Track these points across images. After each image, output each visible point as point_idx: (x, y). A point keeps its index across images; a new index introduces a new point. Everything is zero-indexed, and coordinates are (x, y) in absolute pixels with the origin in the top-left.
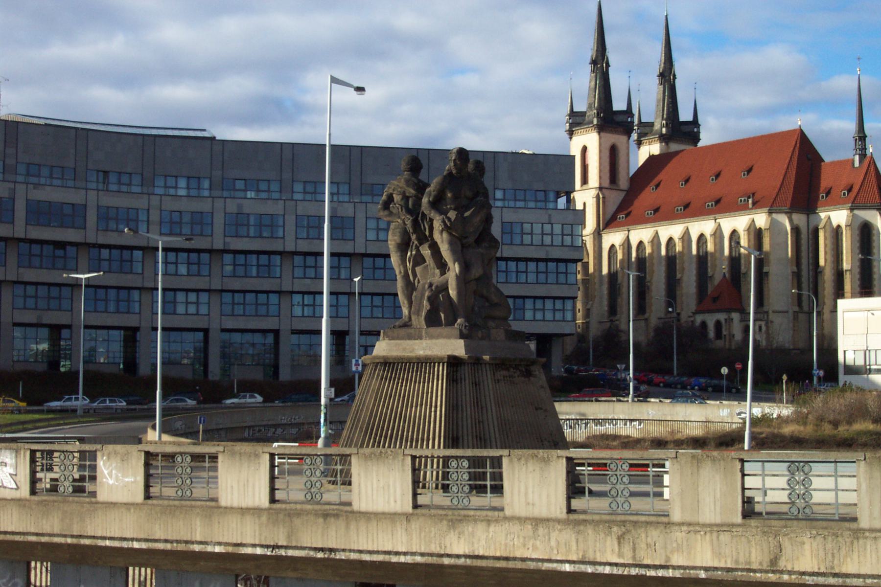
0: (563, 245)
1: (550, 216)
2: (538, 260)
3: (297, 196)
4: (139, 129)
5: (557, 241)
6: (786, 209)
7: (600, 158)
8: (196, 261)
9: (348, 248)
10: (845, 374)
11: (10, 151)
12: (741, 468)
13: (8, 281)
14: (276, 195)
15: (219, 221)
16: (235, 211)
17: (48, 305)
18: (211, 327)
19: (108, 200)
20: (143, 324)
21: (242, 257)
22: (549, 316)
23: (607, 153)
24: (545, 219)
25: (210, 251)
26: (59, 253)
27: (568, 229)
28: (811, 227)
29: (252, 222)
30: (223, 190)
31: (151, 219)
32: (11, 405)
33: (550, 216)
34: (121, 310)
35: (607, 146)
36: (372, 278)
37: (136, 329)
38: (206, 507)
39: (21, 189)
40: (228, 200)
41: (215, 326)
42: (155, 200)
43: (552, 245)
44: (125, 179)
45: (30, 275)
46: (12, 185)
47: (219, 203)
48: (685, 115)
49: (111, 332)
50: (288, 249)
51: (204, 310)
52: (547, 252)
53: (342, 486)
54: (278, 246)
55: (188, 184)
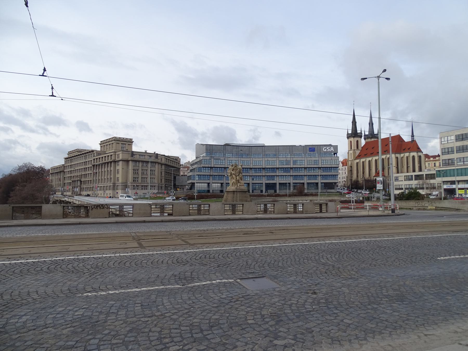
5: (333, 163)
6: (394, 153)
7: (291, 149)
10: (276, 183)
12: (312, 194)
20: (211, 182)
21: (296, 168)
23: (350, 143)
25: (263, 168)
28: (401, 157)
34: (408, 176)
37: (209, 183)
38: (46, 202)
45: (268, 174)
47: (264, 159)
48: (376, 132)
49: (218, 184)
50: (320, 167)
51: (248, 179)
53: (444, 201)
54: (289, 166)
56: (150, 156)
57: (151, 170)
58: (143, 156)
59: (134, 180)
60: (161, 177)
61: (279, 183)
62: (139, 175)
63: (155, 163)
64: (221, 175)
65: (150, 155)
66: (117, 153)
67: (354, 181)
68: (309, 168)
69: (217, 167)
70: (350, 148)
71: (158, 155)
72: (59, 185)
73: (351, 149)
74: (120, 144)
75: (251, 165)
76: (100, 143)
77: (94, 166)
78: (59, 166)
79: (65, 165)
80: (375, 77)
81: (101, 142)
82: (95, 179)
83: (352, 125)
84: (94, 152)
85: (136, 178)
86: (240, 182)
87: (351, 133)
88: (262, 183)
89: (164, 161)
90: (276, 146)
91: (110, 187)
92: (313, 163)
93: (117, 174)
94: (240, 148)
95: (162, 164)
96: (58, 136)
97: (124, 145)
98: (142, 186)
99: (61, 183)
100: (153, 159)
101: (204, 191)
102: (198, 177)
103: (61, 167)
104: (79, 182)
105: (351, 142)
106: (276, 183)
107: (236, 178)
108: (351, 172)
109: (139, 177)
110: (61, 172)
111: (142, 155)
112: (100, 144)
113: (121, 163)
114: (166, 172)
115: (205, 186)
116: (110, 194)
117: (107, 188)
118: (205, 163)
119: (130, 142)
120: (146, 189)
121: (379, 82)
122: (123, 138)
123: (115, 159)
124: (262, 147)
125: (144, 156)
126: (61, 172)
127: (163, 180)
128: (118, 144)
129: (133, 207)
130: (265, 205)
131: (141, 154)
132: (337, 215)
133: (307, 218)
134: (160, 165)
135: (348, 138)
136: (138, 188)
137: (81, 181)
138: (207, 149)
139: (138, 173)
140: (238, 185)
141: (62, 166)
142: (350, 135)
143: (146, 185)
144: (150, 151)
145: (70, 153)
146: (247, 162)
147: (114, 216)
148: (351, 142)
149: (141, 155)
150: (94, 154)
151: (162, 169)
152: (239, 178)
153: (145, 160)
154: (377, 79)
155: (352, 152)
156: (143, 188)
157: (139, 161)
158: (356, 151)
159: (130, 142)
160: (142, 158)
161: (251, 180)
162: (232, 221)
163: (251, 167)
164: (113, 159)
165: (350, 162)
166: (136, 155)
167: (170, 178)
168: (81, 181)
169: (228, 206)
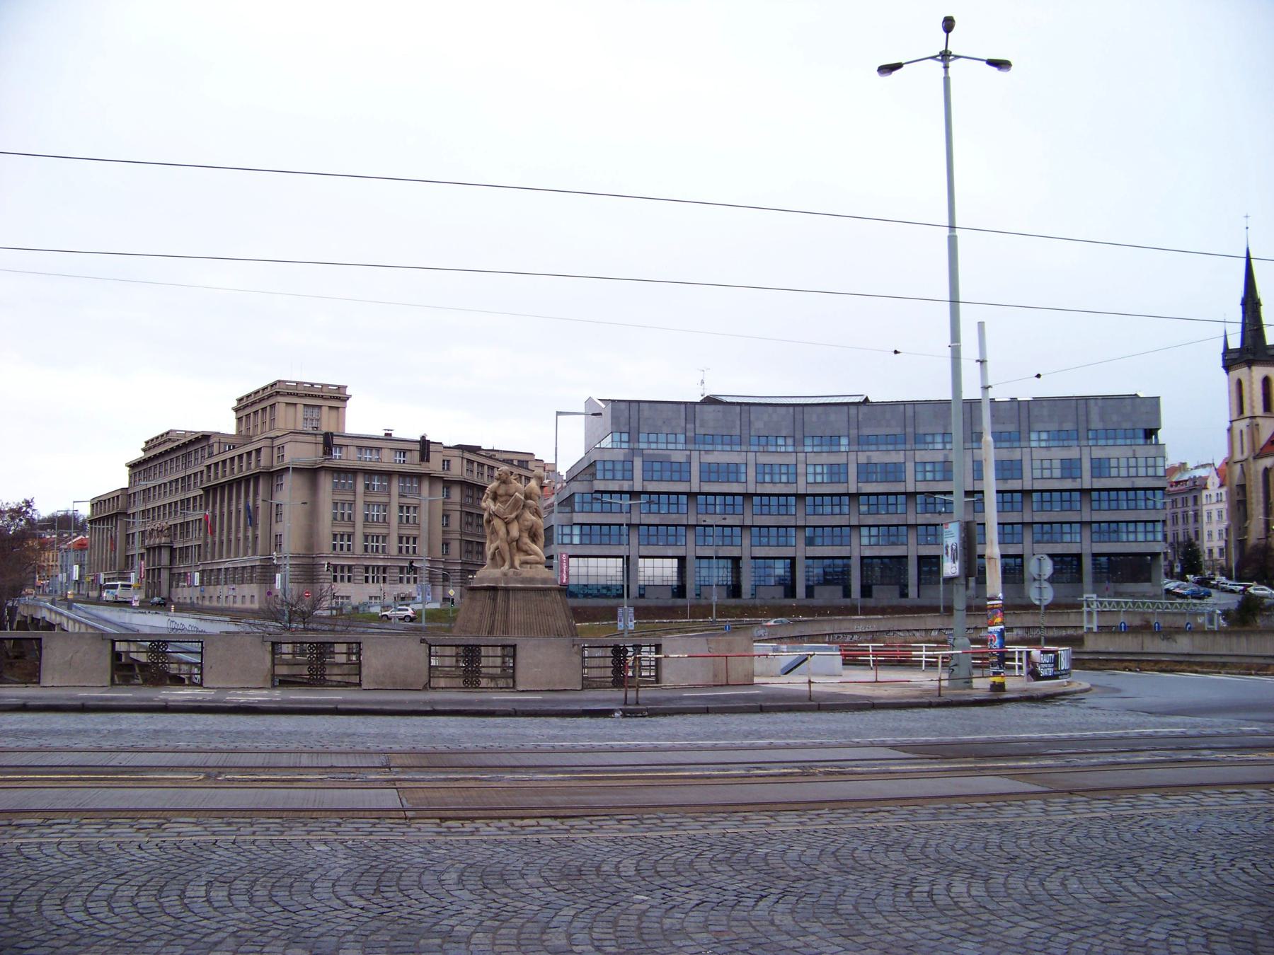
0: (1147, 476)
1: (1134, 451)
2: (1127, 490)
3: (1033, 444)
4: (793, 399)
8: (838, 503)
9: (1014, 485)
11: (690, 426)
13: (633, 525)
14: (790, 449)
15: (853, 470)
16: (865, 462)
17: (1146, 537)
18: (909, 554)
19: (763, 459)
22: (1141, 537)
23: (1234, 387)
24: (1130, 454)
26: (930, 500)
27: (1151, 462)
29: (879, 470)
30: (972, 442)
31: (798, 471)
32: (1188, 619)
33: (1134, 451)
35: (1235, 381)
36: (1143, 508)
37: (740, 558)
39: (695, 455)
40: (758, 454)
41: (634, 553)
42: (801, 456)
43: (1137, 476)
44: (763, 440)
46: (688, 453)
47: (852, 456)
49: (610, 560)
52: (1133, 482)
55: (943, 439)
56: (404, 452)
57: (401, 507)
58: (374, 451)
59: (366, 547)
60: (444, 532)
61: (920, 558)
62: (354, 526)
63: (419, 477)
64: (676, 526)
65: (402, 447)
66: (277, 442)
67: (1255, 547)
68: (1042, 491)
69: (659, 493)
70: (1235, 408)
71: (432, 448)
72: (111, 565)
73: (1241, 410)
74: (300, 408)
75: (801, 480)
76: (235, 404)
77: (206, 490)
78: (111, 496)
79: (130, 492)
80: (934, 58)
81: (240, 400)
82: (209, 540)
83: (1244, 312)
84: (212, 441)
85: (342, 536)
86: (525, 547)
87: (1238, 346)
88: (849, 558)
89: (457, 470)
90: (904, 403)
91: (252, 573)
92: (1057, 473)
93: (277, 522)
94: (812, 416)
95: (448, 484)
96: (1241, 431)
97: (316, 410)
98: (367, 568)
99: (94, 560)
100: (412, 464)
101: (604, 591)
102: (581, 535)
103: (118, 497)
104: (165, 555)
105: (1239, 383)
106: (906, 557)
107: (508, 532)
108: (1242, 508)
109: (388, 534)
110: (117, 516)
111: (371, 448)
112: (237, 410)
113: (289, 480)
114: (468, 513)
115: (668, 572)
116: (244, 596)
117: (243, 574)
118: (609, 475)
119: (337, 397)
120: (412, 580)
121: (947, 80)
122: (312, 385)
123: (270, 465)
124: (845, 408)
125: (379, 449)
126: (116, 515)
127: (455, 547)
128: (291, 409)
129: (202, 648)
130: (472, 651)
131: (365, 444)
132: (626, 703)
133: (707, 711)
134: (439, 488)
135: (1228, 366)
136: (384, 578)
137: (172, 550)
138: (615, 419)
139: (414, 523)
140: (517, 563)
141: (119, 493)
142: (1234, 356)
143: (381, 563)
144: (408, 430)
145: (150, 445)
146: (819, 469)
147: (168, 682)
148: (1239, 383)
149: (367, 448)
150: (211, 446)
151: (452, 503)
152: (520, 531)
153: (378, 466)
154: (941, 64)
155: (1242, 425)
156: (370, 575)
157: (354, 472)
158: (1260, 421)
159: (337, 397)
160: (370, 461)
161: (801, 544)
162: (327, 717)
163: (802, 491)
164: (262, 463)
165: (1238, 467)
166: (344, 449)
167: (478, 536)
168: (172, 550)
169: (449, 651)
